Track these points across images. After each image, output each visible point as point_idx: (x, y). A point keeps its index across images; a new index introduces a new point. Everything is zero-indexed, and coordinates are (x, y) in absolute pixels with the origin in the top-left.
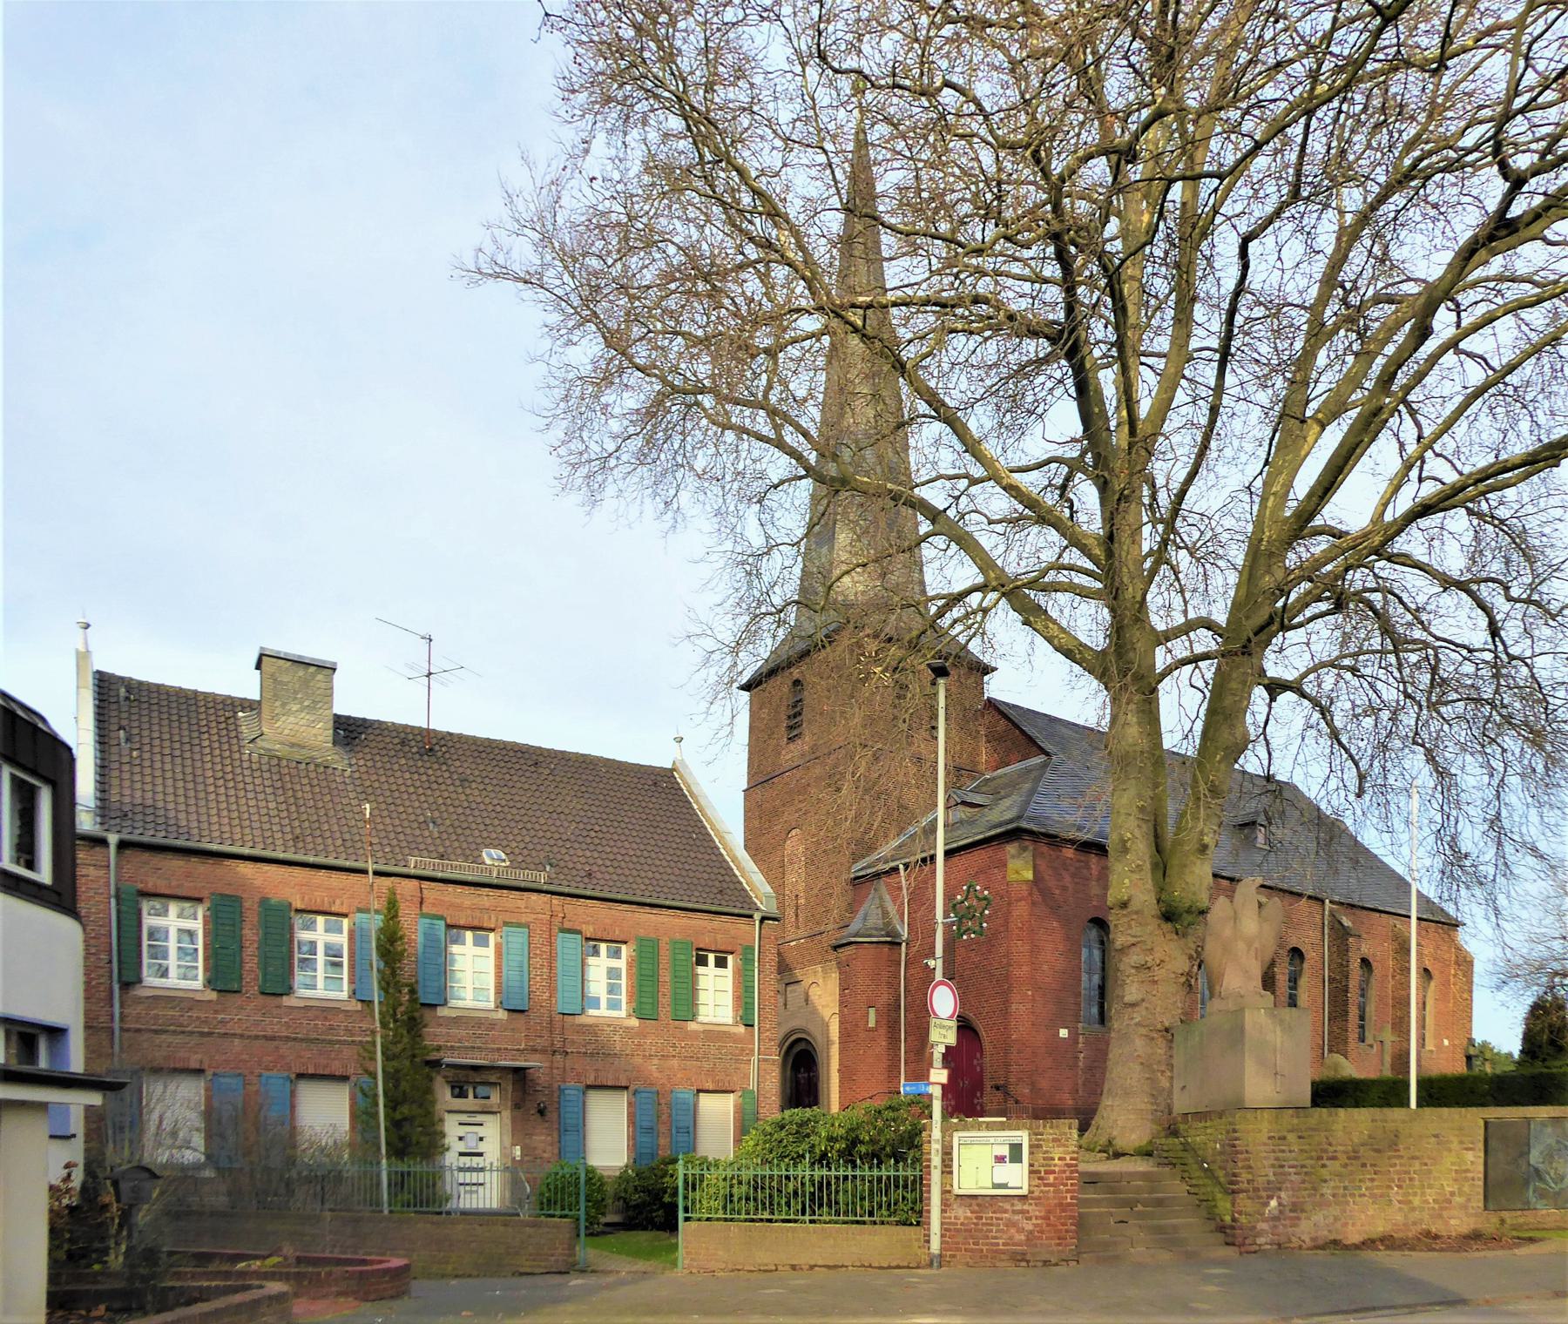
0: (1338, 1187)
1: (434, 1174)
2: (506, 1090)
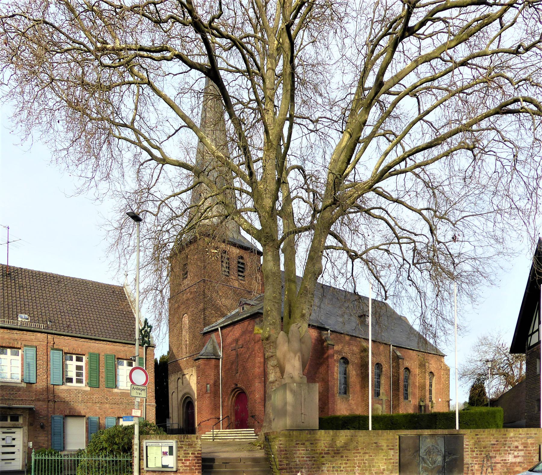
0: (330, 467)
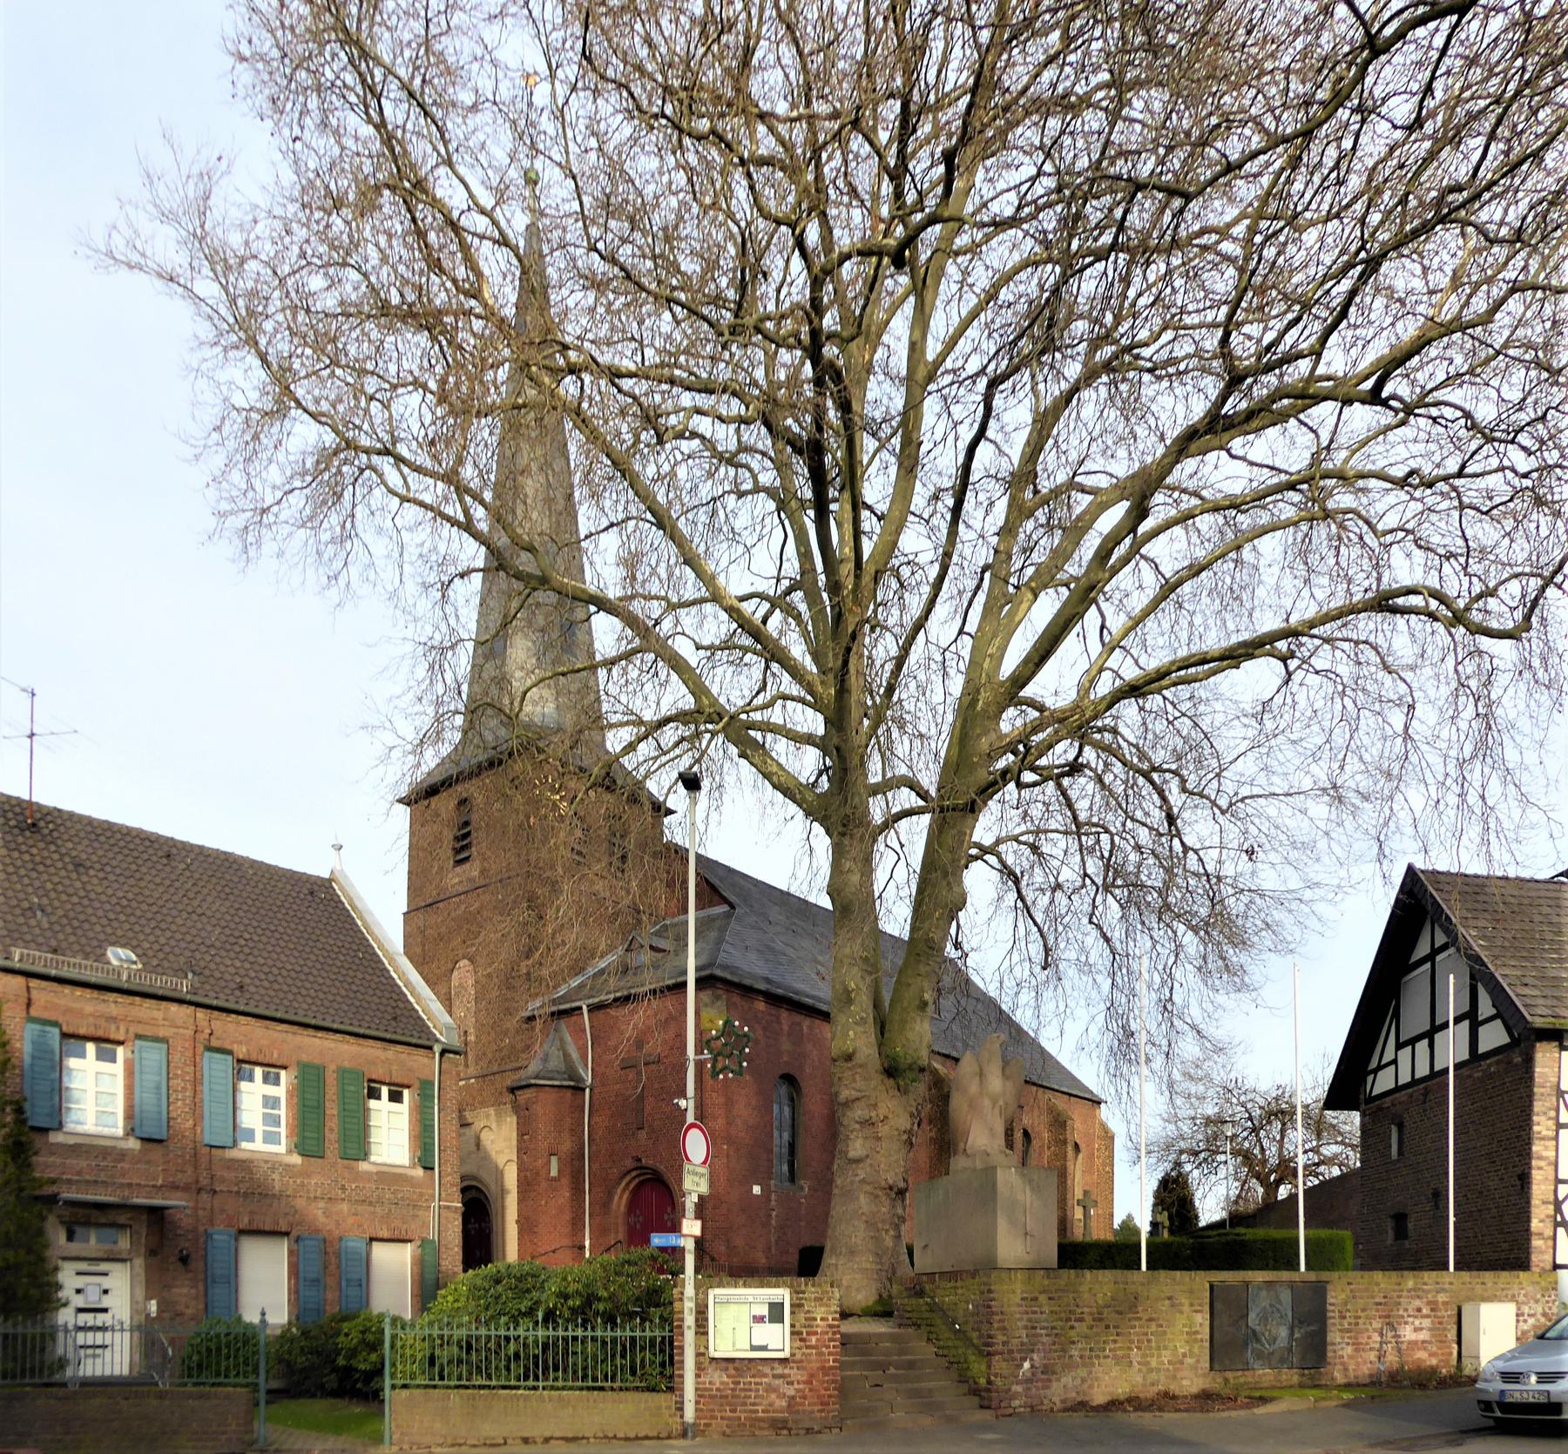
1: (43, 1336)
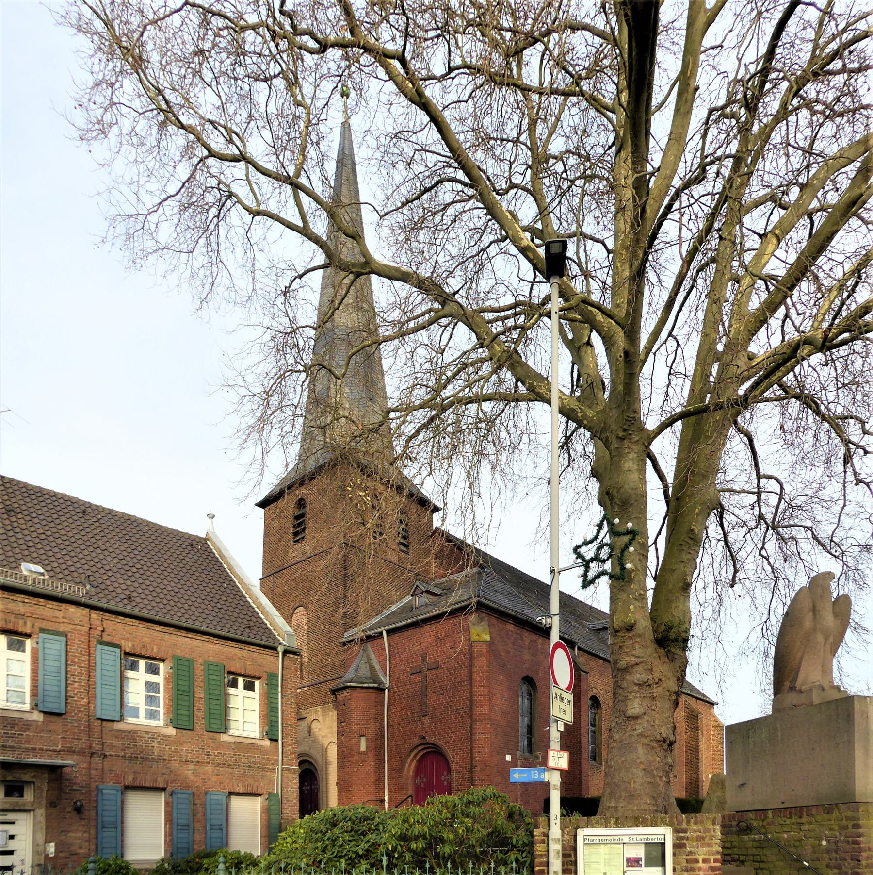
2: (40, 788)
